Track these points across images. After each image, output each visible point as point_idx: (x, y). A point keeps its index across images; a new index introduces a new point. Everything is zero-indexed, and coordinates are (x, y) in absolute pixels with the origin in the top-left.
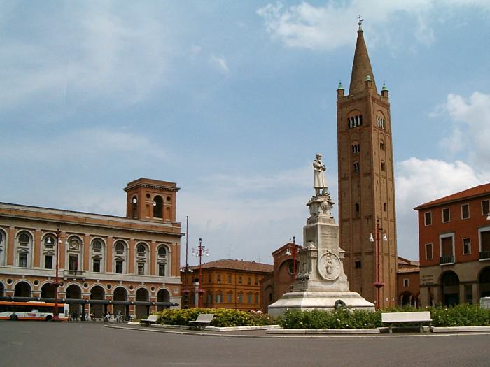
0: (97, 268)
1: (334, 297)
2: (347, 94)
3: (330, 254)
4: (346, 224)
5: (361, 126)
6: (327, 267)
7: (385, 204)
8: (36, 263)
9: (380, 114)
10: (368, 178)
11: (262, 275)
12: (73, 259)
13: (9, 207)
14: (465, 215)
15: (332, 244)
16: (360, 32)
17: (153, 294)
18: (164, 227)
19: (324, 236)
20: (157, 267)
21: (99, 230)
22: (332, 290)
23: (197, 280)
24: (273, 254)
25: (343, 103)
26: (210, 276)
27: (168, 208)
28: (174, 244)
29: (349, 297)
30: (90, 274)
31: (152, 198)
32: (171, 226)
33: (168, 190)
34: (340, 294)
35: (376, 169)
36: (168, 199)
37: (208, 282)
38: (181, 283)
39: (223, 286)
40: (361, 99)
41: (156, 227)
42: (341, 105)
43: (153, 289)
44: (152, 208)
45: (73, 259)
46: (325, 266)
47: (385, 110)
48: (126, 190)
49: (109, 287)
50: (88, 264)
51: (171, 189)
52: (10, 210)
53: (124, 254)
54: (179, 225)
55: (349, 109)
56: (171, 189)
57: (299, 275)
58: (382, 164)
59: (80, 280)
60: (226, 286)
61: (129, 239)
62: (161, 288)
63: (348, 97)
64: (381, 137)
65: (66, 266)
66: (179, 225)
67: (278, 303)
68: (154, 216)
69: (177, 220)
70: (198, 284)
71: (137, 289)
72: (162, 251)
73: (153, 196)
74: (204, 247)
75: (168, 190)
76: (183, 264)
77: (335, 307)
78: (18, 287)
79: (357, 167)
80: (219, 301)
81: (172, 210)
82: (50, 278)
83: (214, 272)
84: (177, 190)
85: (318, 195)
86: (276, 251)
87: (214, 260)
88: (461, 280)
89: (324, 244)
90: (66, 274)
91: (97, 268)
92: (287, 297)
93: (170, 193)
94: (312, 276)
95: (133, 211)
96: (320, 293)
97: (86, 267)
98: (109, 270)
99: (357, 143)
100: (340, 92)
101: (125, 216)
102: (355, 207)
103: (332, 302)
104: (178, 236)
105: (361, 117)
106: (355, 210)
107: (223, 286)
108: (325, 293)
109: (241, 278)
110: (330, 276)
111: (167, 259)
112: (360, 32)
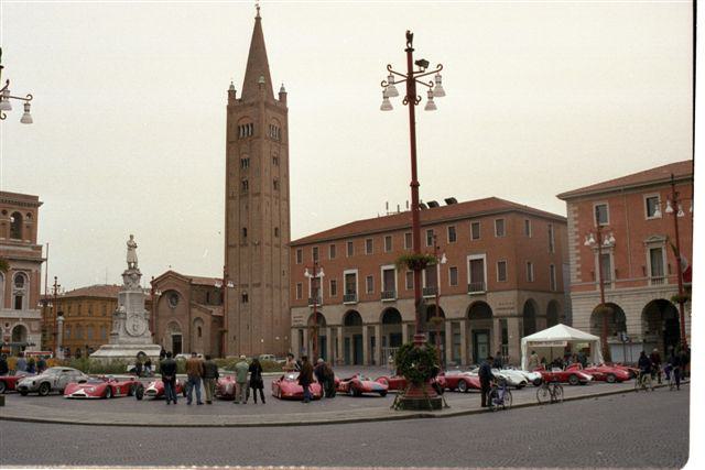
2: (238, 96)
4: (233, 251)
5: (256, 127)
7: (276, 229)
9: (274, 122)
10: (257, 198)
14: (333, 255)
16: (258, 19)
17: (7, 331)
18: (22, 252)
19: (131, 301)
20: (13, 299)
23: (60, 314)
25: (234, 107)
28: (34, 271)
29: (151, 349)
32: (30, 250)
33: (29, 205)
34: (143, 346)
35: (267, 188)
37: (76, 314)
38: (40, 317)
40: (252, 105)
41: (14, 252)
42: (231, 109)
43: (7, 325)
44: (9, 226)
47: (281, 117)
51: (31, 203)
54: (40, 248)
55: (240, 115)
56: (31, 203)
57: (114, 331)
58: (275, 183)
62: (16, 324)
63: (240, 100)
64: (275, 149)
66: (40, 248)
67: (94, 354)
68: (11, 237)
69: (39, 243)
70: (61, 318)
72: (20, 280)
73: (10, 212)
75: (29, 205)
76: (43, 292)
77: (138, 356)
79: (245, 184)
81: (32, 229)
85: (130, 268)
88: (403, 319)
89: (132, 308)
92: (104, 349)
94: (121, 333)
96: (127, 346)
99: (246, 156)
100: (232, 93)
102: (242, 231)
103: (135, 353)
104: (39, 262)
105: (252, 125)
106: (242, 235)
108: (132, 346)
111: (26, 288)
112: (258, 19)
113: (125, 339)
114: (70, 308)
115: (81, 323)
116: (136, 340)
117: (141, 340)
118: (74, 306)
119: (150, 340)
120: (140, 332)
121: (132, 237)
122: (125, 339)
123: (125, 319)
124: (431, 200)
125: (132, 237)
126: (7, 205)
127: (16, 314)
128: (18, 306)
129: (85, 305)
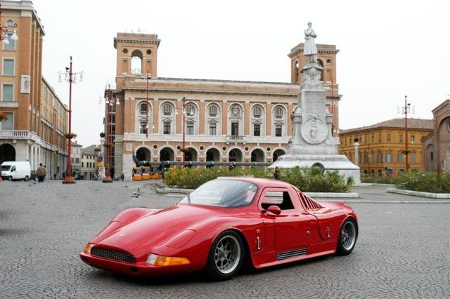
0: (257, 133)
1: (313, 160)
3: (315, 118)
6: (311, 131)
8: (202, 131)
11: (106, 146)
12: (235, 127)
13: (176, 82)
15: (317, 109)
17: (202, 153)
19: (308, 101)
21: (258, 97)
22: (317, 153)
24: (433, 111)
26: (380, 135)
27: (328, 70)
29: (333, 160)
30: (251, 138)
31: (315, 63)
33: (328, 53)
36: (329, 61)
39: (393, 145)
41: (168, 84)
45: (235, 127)
46: (309, 130)
48: (290, 56)
49: (269, 149)
50: (249, 129)
52: (177, 85)
53: (283, 118)
59: (241, 144)
60: (396, 145)
61: (287, 104)
65: (228, 132)
70: (357, 144)
71: (252, 150)
74: (409, 104)
75: (328, 53)
78: (162, 152)
80: (389, 160)
82: (213, 144)
83: (384, 131)
84: (336, 52)
86: (436, 109)
87: (380, 121)
90: (228, 138)
91: (257, 133)
93: (331, 55)
95: (297, 75)
96: (301, 156)
97: (247, 132)
98: (268, 133)
101: (290, 81)
103: (310, 164)
107: (393, 145)
109: (389, 135)
110: (315, 140)
113: (301, 148)
114: (373, 137)
115: (381, 149)
116: (315, 148)
117: (320, 148)
118: (376, 134)
119: (334, 149)
120: (320, 138)
121: (310, 24)
122: (301, 148)
123: (300, 123)
124: (360, 221)
125: (310, 24)
126: (128, 44)
127: (143, 138)
128: (145, 131)
129: (384, 134)
